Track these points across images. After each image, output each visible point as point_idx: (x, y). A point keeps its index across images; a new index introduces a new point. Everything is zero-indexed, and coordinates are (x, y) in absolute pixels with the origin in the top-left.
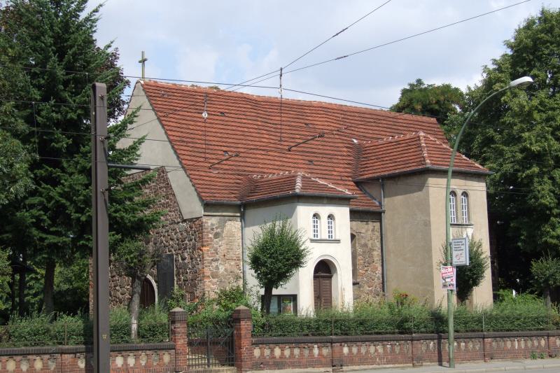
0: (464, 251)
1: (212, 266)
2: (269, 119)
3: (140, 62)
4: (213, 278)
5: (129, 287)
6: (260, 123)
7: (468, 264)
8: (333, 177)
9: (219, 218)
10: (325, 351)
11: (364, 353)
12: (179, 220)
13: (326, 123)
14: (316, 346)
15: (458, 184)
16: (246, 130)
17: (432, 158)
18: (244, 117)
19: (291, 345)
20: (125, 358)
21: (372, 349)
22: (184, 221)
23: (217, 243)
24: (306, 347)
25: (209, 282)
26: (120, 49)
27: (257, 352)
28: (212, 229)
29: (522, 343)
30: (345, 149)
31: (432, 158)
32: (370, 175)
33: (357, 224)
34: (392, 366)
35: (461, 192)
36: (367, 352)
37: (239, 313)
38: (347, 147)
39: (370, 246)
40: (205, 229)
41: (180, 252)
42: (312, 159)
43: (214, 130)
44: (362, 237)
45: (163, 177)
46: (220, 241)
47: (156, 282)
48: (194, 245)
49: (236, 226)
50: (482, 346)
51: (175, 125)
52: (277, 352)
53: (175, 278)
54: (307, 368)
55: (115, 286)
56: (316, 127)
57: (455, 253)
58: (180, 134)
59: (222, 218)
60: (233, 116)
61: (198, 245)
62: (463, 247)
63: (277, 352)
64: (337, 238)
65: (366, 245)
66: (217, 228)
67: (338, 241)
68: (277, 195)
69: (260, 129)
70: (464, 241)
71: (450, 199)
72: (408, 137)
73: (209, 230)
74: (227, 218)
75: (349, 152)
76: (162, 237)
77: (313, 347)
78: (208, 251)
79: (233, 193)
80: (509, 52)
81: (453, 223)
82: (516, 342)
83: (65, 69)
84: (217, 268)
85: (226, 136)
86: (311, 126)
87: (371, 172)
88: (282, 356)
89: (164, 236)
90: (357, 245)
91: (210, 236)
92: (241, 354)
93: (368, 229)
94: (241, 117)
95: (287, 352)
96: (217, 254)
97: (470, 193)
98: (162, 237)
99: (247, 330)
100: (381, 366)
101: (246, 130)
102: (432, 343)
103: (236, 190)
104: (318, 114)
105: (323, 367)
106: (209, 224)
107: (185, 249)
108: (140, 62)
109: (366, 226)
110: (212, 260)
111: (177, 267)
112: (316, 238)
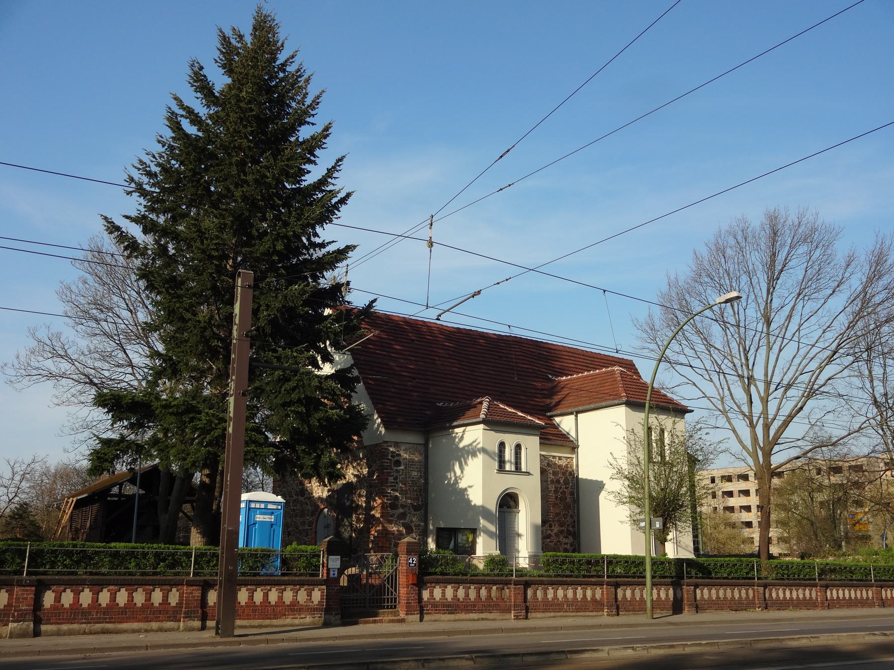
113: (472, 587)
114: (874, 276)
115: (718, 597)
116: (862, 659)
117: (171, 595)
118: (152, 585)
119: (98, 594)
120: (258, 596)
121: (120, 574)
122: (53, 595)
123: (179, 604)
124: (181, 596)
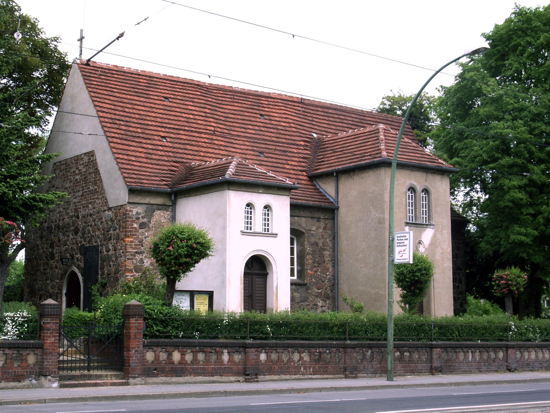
0: (408, 247)
1: (136, 259)
2: (220, 108)
3: (78, 40)
4: (136, 272)
5: (58, 281)
6: (208, 111)
7: (411, 262)
8: (285, 170)
9: (146, 206)
10: (237, 357)
11: (285, 361)
12: (105, 208)
13: (284, 116)
14: (225, 351)
15: (418, 180)
16: (191, 116)
18: (191, 104)
19: (193, 349)
21: (296, 357)
22: (110, 209)
23: (143, 234)
24: (213, 351)
25: (132, 276)
27: (150, 356)
29: (477, 354)
30: (302, 143)
32: (326, 170)
33: (304, 223)
34: (319, 376)
35: (422, 188)
36: (290, 360)
37: (129, 309)
38: (304, 141)
39: (321, 245)
40: (130, 218)
41: (105, 243)
42: (168, 96)
43: (153, 115)
44: (312, 235)
45: (92, 161)
46: (146, 231)
47: (82, 275)
48: (118, 234)
49: (166, 216)
50: (429, 357)
51: (108, 106)
53: (100, 272)
54: (213, 376)
55: (46, 280)
56: (273, 118)
57: (397, 249)
58: (113, 117)
59: (149, 206)
60: (178, 101)
61: (122, 235)
62: (406, 242)
63: (176, 356)
64: (274, 232)
65: (316, 244)
66: (143, 217)
67: (275, 235)
68: (207, 182)
69: (207, 117)
70: (407, 235)
71: (409, 195)
72: (368, 130)
73: (134, 219)
74: (155, 207)
75: (307, 146)
76: (89, 227)
77: (222, 352)
78: (132, 242)
79: (164, 181)
80: (486, 44)
81: (408, 221)
82: (470, 353)
84: (142, 261)
85: (167, 121)
86: (266, 117)
87: (326, 166)
88: (182, 361)
89: (91, 226)
90: (306, 243)
91: (135, 225)
92: (129, 357)
93: (315, 227)
94: (188, 103)
95: (163, 356)
97: (432, 191)
98: (89, 227)
99: (138, 329)
100: (306, 377)
101: (191, 116)
102: (370, 351)
103: (168, 177)
104: (276, 106)
105: (233, 376)
106: (134, 213)
107: (110, 239)
108: (78, 40)
109: (318, 224)
110: (136, 252)
111: (101, 260)
112: (249, 231)
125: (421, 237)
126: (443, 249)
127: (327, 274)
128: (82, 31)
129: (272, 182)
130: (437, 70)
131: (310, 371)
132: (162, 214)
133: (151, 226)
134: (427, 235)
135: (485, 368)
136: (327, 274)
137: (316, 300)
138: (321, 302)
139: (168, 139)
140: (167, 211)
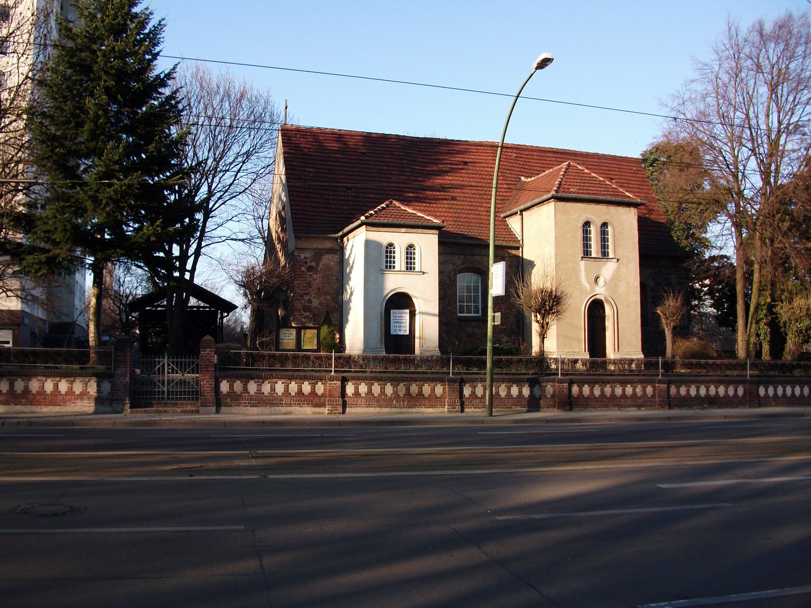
1: (305, 299)
4: (305, 311)
17: (301, 153)
20: (727, 388)
26: (655, 135)
28: (306, 263)
31: (301, 153)
52: (780, 390)
73: (302, 263)
83: (114, 118)
84: (310, 301)
91: (303, 269)
95: (789, 390)
96: (311, 287)
106: (302, 258)
113: (693, 386)
114: (808, 37)
115: (775, 394)
116: (73, 425)
117: (627, 389)
118: (45, 376)
119: (261, 385)
120: (789, 390)
121: (787, 376)
122: (685, 388)
123: (654, 396)
124: (654, 391)
125: (600, 271)
126: (628, 283)
127: (513, 310)
128: (286, 101)
129: (430, 224)
130: (516, 95)
131: (404, 405)
132: (330, 258)
133: (319, 269)
134: (608, 269)
135: (774, 404)
136: (513, 310)
137: (500, 335)
138: (506, 338)
139: (353, 190)
140: (336, 254)
